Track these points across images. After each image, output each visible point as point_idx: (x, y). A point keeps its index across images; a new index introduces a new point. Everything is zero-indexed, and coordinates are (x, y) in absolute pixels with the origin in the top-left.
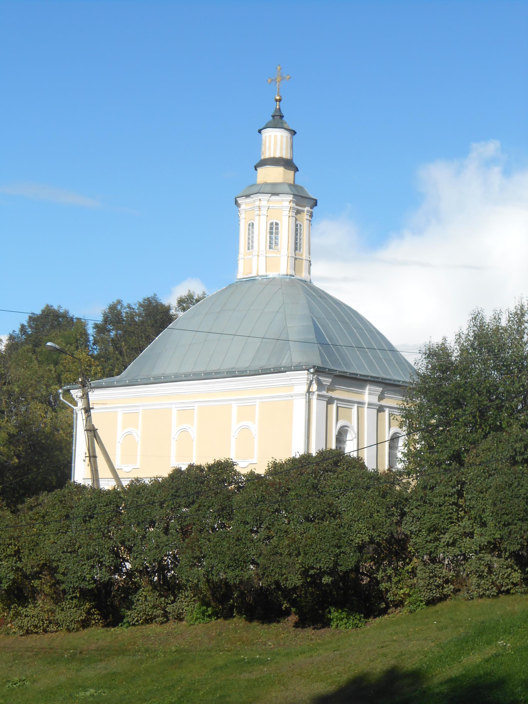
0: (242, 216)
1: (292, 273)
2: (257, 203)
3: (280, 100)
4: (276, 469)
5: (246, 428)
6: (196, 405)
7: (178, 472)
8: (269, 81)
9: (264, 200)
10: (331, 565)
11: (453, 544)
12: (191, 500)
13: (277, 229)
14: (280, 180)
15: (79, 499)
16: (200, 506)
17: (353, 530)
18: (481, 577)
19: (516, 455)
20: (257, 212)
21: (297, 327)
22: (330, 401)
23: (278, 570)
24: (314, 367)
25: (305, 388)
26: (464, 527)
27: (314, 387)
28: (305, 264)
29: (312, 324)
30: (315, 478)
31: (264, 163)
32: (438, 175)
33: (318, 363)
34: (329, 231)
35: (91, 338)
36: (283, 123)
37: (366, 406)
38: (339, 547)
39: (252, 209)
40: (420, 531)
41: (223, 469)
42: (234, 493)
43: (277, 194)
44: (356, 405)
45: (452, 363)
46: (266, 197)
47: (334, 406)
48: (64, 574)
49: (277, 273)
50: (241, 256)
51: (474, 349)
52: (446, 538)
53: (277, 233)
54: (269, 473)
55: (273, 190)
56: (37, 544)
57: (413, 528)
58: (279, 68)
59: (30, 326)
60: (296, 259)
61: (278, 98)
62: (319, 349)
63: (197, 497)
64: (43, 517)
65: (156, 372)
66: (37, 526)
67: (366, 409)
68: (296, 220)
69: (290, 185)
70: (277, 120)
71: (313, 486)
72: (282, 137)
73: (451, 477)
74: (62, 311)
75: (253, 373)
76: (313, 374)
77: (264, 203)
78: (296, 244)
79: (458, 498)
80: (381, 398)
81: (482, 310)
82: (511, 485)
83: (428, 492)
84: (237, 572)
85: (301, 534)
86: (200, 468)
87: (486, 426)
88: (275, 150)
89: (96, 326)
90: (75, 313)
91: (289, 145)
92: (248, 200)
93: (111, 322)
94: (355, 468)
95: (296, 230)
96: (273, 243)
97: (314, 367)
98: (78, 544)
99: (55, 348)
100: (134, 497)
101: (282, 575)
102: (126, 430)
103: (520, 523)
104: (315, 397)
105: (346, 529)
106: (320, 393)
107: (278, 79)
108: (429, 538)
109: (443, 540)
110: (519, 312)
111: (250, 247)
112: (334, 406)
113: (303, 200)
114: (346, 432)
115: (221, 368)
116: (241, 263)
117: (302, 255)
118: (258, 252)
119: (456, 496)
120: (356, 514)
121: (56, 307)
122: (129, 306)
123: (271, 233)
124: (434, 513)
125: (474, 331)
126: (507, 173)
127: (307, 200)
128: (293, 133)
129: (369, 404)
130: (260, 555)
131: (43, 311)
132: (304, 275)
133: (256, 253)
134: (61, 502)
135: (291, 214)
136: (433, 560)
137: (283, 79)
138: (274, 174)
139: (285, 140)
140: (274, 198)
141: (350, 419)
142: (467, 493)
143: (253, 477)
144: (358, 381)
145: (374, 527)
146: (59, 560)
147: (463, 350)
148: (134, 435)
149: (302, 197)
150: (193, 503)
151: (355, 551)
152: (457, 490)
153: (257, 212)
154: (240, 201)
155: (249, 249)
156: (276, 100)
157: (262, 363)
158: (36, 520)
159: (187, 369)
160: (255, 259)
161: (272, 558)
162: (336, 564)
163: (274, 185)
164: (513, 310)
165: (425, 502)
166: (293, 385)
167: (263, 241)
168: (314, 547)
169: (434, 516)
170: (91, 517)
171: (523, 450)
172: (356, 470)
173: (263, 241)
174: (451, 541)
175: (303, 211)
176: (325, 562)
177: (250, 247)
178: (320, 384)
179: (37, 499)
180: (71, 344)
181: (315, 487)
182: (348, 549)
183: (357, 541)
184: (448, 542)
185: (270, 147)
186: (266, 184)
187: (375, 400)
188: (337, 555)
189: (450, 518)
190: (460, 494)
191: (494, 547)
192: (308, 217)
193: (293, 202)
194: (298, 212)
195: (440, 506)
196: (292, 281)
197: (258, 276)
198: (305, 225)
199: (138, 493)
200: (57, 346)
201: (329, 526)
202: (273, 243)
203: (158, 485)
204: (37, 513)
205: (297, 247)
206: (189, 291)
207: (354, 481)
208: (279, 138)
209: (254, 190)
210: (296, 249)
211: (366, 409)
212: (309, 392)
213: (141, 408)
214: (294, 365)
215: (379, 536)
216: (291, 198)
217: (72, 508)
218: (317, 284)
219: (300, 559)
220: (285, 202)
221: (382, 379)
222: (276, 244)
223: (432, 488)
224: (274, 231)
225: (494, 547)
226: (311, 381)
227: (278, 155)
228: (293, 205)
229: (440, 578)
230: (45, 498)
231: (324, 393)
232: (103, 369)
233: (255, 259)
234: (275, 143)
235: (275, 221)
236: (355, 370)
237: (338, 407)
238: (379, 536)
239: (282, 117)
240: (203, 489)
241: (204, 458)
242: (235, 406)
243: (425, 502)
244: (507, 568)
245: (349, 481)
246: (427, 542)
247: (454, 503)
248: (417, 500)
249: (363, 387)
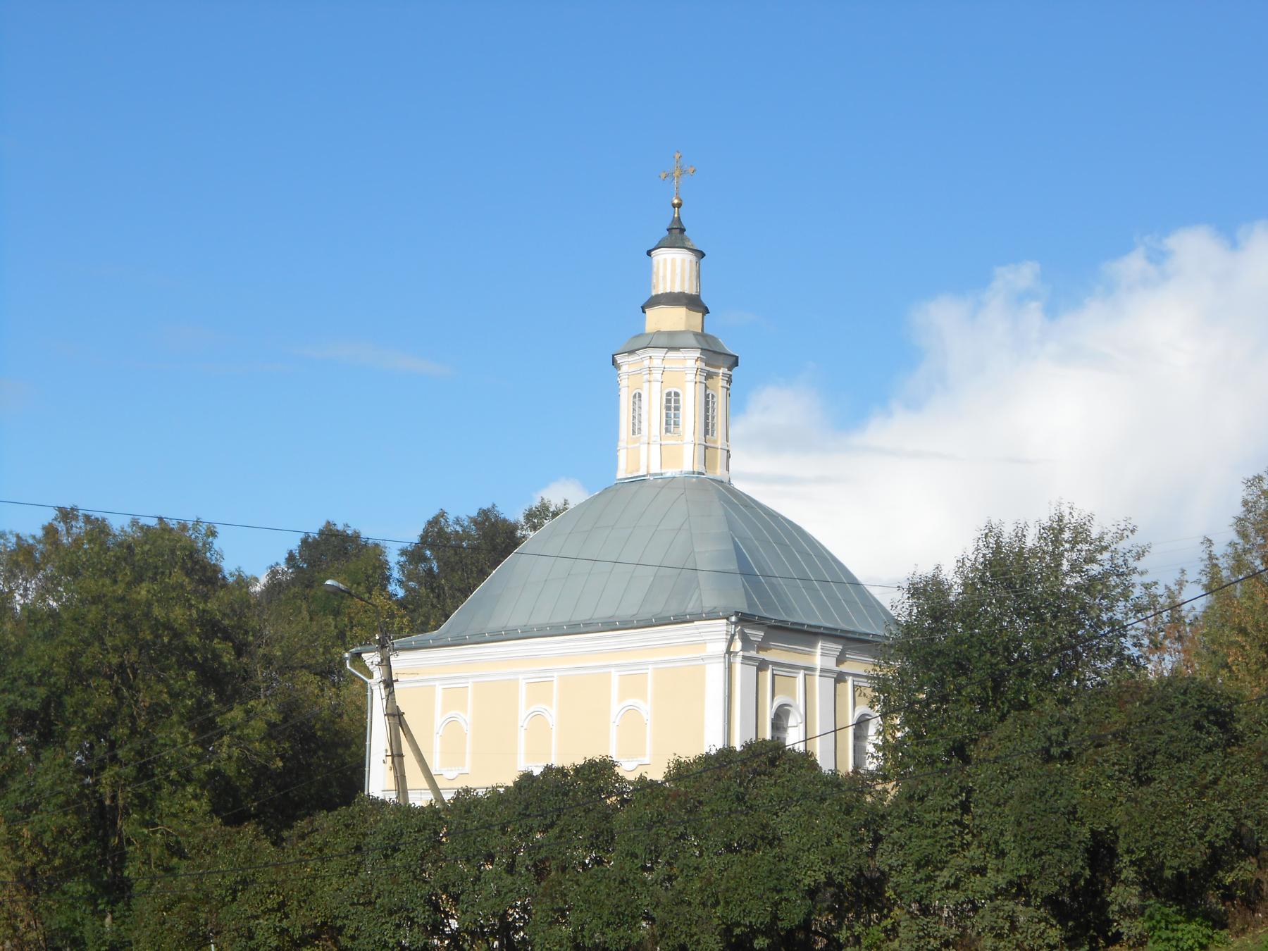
0: (624, 382)
1: (702, 469)
2: (647, 363)
3: (679, 205)
4: (681, 772)
5: (632, 710)
6: (555, 674)
7: (527, 778)
8: (663, 176)
9: (656, 358)
10: (768, 919)
11: (956, 886)
12: (548, 822)
13: (677, 401)
14: (681, 328)
15: (376, 822)
16: (562, 831)
17: (801, 864)
18: (999, 936)
19: (1051, 745)
20: (647, 377)
21: (710, 551)
22: (762, 666)
23: (685, 928)
24: (736, 613)
25: (723, 646)
26: (972, 860)
27: (738, 645)
28: (721, 455)
29: (731, 547)
30: (740, 784)
31: (655, 301)
32: (942, 318)
33: (744, 608)
34: (777, 406)
35: (396, 574)
36: (683, 240)
37: (818, 673)
38: (779, 891)
39: (639, 372)
40: (904, 865)
41: (598, 773)
42: (615, 810)
43: (677, 349)
44: (802, 672)
45: (950, 605)
46: (660, 353)
47: (769, 673)
48: (353, 938)
49: (678, 470)
50: (622, 444)
51: (984, 583)
52: (944, 876)
53: (677, 409)
54: (668, 778)
55: (670, 342)
56: (312, 892)
57: (893, 862)
58: (677, 156)
59: (301, 556)
60: (706, 448)
61: (676, 201)
63: (558, 816)
64: (321, 850)
65: (494, 625)
66: (312, 864)
67: (817, 678)
68: (706, 387)
69: (696, 334)
70: (676, 236)
71: (737, 797)
72: (683, 261)
73: (951, 780)
74: (349, 532)
75: (642, 623)
76: (736, 624)
77: (657, 362)
78: (706, 425)
79: (962, 815)
80: (840, 660)
81: (1002, 523)
82: (1044, 793)
83: (915, 804)
84: (621, 932)
85: (720, 872)
86: (561, 771)
87: (1003, 703)
89: (403, 552)
90: (369, 532)
91: (694, 273)
92: (632, 358)
93: (432, 546)
94: (802, 768)
95: (707, 403)
97: (736, 613)
98: (375, 891)
99: (338, 588)
100: (461, 817)
101: (692, 936)
102: (448, 715)
103: (1058, 851)
104: (738, 659)
105: (789, 863)
106: (747, 654)
107: (677, 173)
108: (918, 877)
109: (940, 880)
110: (1055, 525)
112: (769, 673)
113: (717, 357)
114: (787, 713)
115: (596, 616)
116: (622, 456)
117: (715, 442)
119: (959, 811)
120: (805, 840)
121: (340, 527)
122: (457, 521)
123: (668, 408)
124: (926, 837)
125: (984, 555)
126: (1051, 311)
127: (722, 357)
128: (701, 255)
129: (822, 670)
130: (657, 906)
131: (321, 533)
132: (719, 473)
133: (645, 439)
134: (347, 826)
135: (699, 378)
136: (925, 911)
137: (683, 172)
138: (673, 319)
140: (672, 354)
141: (792, 694)
142: (976, 806)
143: (644, 785)
144: (805, 635)
145: (833, 859)
146: (346, 917)
147: (968, 585)
148: (459, 721)
149: (715, 352)
150: (552, 825)
151: (804, 898)
152: (961, 802)
153: (647, 377)
154: (619, 359)
155: (634, 433)
156: (674, 206)
157: (656, 609)
158: (310, 854)
159: (540, 619)
160: (644, 448)
161: (675, 909)
162: (775, 918)
163: (671, 334)
164: (1046, 523)
165: (911, 821)
166: (705, 642)
167: (655, 422)
168: (740, 891)
169: (925, 842)
170: (395, 850)
171: (1061, 738)
172: (803, 771)
173: (655, 422)
174: (952, 881)
175: (717, 374)
176: (758, 916)
178: (746, 641)
179: (311, 823)
180: (359, 584)
181: (740, 799)
182: (792, 895)
183: (806, 882)
184: (948, 882)
185: (664, 277)
186: (659, 333)
187: (831, 663)
188: (776, 904)
189: (951, 845)
190: (965, 807)
191: (1019, 889)
192: (725, 384)
193: (702, 360)
194: (709, 376)
195: (935, 826)
196: (701, 482)
197: (648, 474)
198: (720, 395)
199: (468, 811)
200: (341, 586)
201: (762, 859)
203: (498, 798)
204: (312, 844)
205: (708, 429)
206: (494, 506)
207: (800, 789)
208: (678, 263)
209: (641, 343)
210: (706, 432)
211: (817, 678)
212: (729, 652)
214: (706, 610)
215: (841, 873)
216: (697, 354)
217: (365, 835)
218: (739, 485)
219: (719, 911)
220: (689, 361)
221: (842, 631)
222: (677, 424)
223: (922, 799)
225: (1019, 889)
226: (732, 636)
227: (677, 290)
228: (701, 365)
229: (935, 938)
230: (324, 820)
231: (753, 653)
232: (412, 621)
233: (644, 448)
234: (672, 269)
235: (673, 390)
236: (800, 617)
237: (773, 675)
238: (841, 873)
239: (682, 230)
240: (569, 801)
241: (568, 756)
242: (615, 676)
243: (911, 821)
244: (1040, 922)
245: (794, 790)
246: (915, 882)
247: (956, 822)
248: (899, 818)
249: (812, 644)
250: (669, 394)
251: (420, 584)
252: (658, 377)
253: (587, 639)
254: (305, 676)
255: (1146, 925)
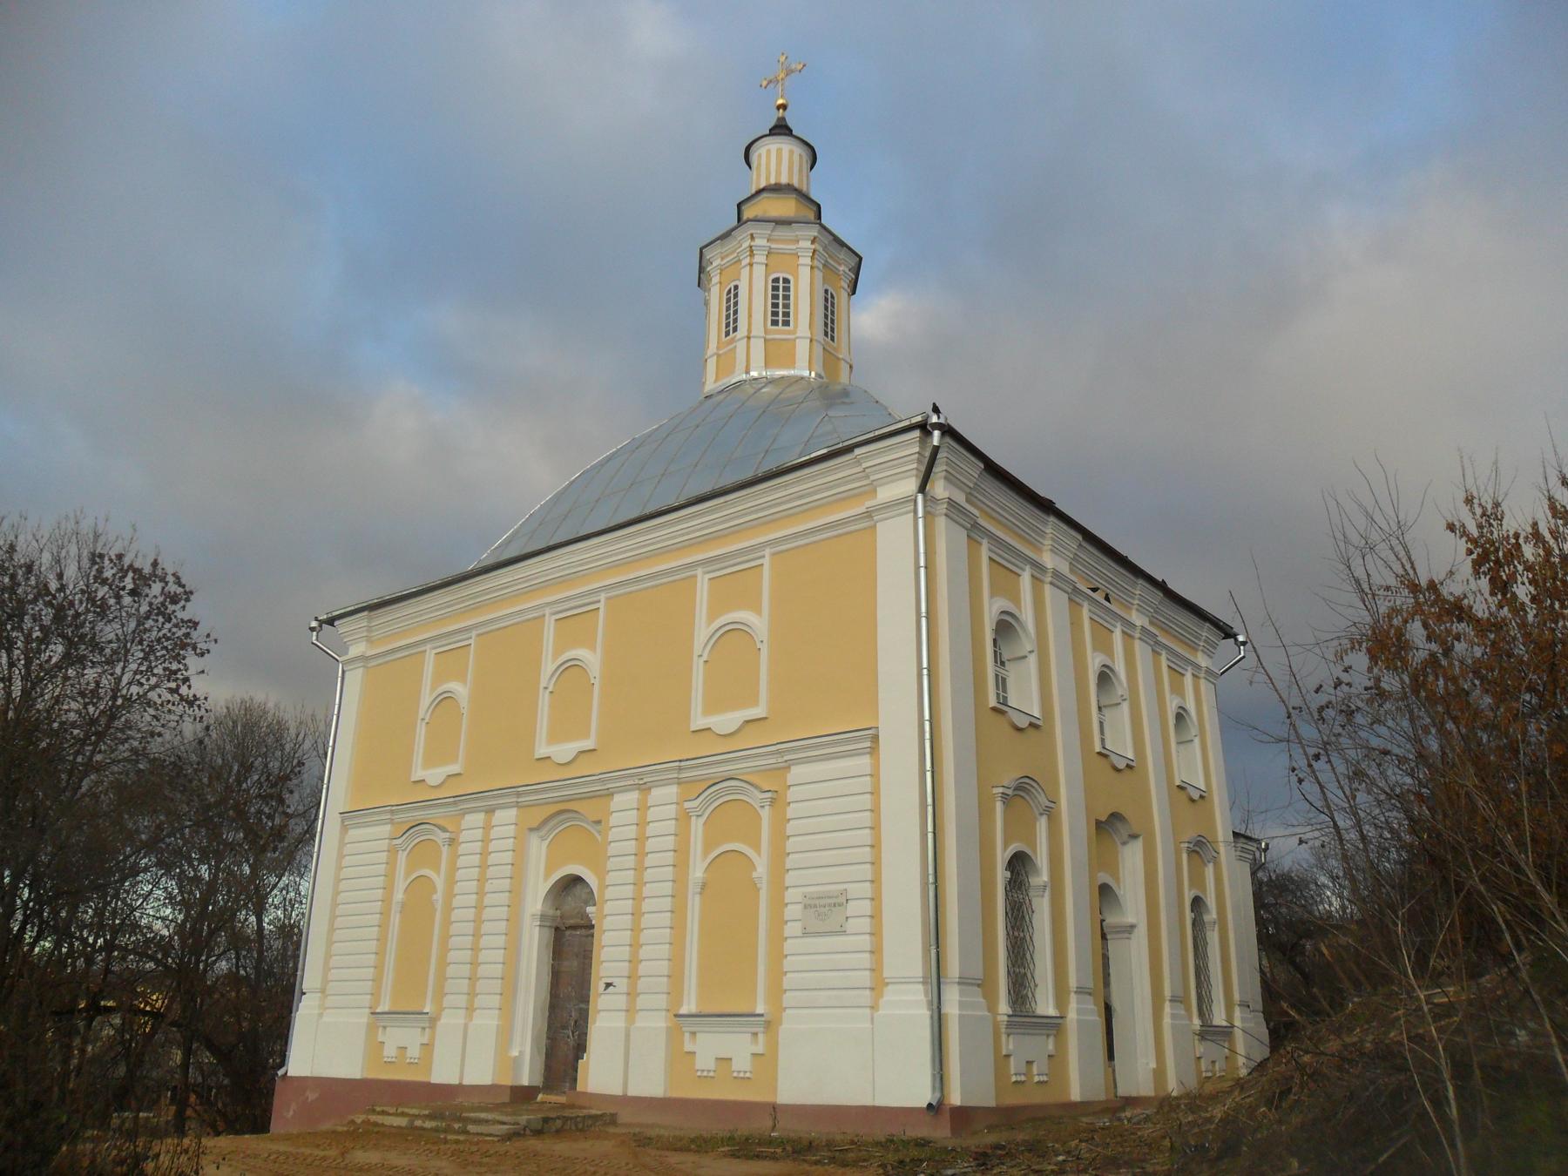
24: (1355, 645)
58: (782, 59)
61: (780, 101)
62: (581, 1108)
72: (791, 152)
88: (778, 173)
96: (780, 313)
111: (731, 326)
118: (749, 331)
139: (796, 158)
160: (741, 346)
177: (731, 326)
202: (780, 313)
213: (603, 596)
224: (781, 310)
227: (784, 180)
235: (781, 276)
242: (703, 581)
250: (776, 280)
251: (1410, 992)
252: (763, 259)
253: (656, 528)
254: (1480, 610)
255: (44, 657)
